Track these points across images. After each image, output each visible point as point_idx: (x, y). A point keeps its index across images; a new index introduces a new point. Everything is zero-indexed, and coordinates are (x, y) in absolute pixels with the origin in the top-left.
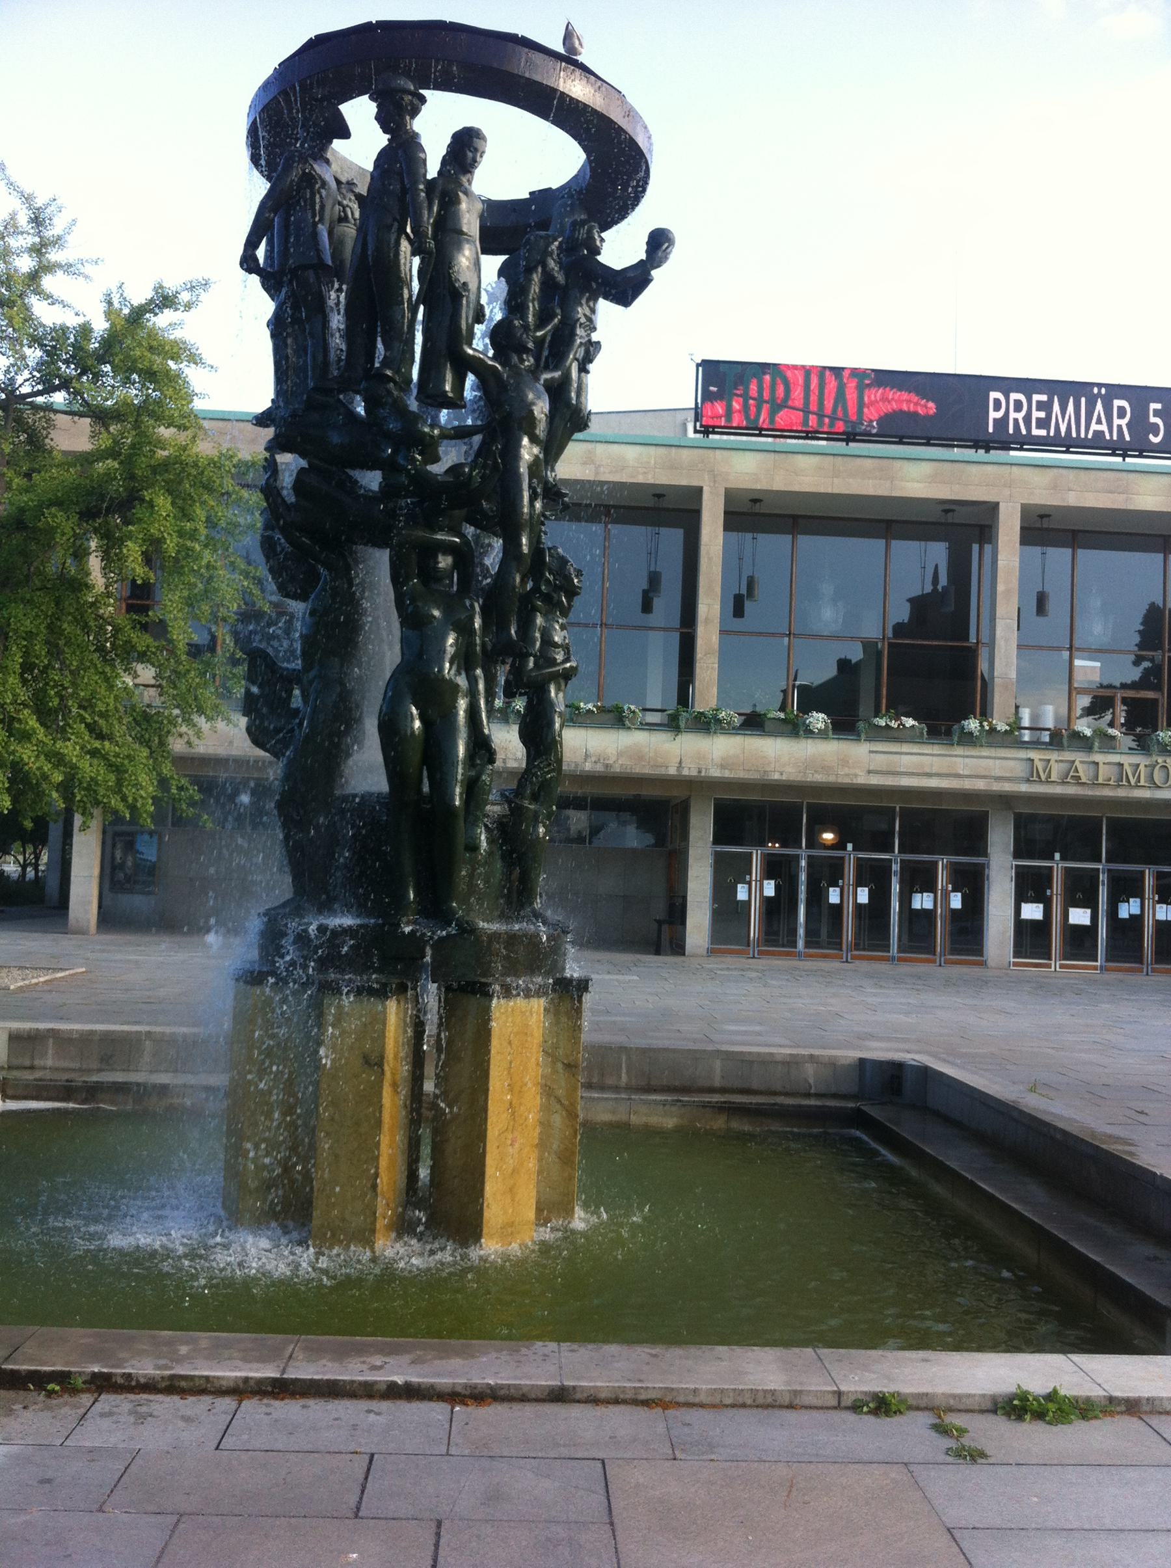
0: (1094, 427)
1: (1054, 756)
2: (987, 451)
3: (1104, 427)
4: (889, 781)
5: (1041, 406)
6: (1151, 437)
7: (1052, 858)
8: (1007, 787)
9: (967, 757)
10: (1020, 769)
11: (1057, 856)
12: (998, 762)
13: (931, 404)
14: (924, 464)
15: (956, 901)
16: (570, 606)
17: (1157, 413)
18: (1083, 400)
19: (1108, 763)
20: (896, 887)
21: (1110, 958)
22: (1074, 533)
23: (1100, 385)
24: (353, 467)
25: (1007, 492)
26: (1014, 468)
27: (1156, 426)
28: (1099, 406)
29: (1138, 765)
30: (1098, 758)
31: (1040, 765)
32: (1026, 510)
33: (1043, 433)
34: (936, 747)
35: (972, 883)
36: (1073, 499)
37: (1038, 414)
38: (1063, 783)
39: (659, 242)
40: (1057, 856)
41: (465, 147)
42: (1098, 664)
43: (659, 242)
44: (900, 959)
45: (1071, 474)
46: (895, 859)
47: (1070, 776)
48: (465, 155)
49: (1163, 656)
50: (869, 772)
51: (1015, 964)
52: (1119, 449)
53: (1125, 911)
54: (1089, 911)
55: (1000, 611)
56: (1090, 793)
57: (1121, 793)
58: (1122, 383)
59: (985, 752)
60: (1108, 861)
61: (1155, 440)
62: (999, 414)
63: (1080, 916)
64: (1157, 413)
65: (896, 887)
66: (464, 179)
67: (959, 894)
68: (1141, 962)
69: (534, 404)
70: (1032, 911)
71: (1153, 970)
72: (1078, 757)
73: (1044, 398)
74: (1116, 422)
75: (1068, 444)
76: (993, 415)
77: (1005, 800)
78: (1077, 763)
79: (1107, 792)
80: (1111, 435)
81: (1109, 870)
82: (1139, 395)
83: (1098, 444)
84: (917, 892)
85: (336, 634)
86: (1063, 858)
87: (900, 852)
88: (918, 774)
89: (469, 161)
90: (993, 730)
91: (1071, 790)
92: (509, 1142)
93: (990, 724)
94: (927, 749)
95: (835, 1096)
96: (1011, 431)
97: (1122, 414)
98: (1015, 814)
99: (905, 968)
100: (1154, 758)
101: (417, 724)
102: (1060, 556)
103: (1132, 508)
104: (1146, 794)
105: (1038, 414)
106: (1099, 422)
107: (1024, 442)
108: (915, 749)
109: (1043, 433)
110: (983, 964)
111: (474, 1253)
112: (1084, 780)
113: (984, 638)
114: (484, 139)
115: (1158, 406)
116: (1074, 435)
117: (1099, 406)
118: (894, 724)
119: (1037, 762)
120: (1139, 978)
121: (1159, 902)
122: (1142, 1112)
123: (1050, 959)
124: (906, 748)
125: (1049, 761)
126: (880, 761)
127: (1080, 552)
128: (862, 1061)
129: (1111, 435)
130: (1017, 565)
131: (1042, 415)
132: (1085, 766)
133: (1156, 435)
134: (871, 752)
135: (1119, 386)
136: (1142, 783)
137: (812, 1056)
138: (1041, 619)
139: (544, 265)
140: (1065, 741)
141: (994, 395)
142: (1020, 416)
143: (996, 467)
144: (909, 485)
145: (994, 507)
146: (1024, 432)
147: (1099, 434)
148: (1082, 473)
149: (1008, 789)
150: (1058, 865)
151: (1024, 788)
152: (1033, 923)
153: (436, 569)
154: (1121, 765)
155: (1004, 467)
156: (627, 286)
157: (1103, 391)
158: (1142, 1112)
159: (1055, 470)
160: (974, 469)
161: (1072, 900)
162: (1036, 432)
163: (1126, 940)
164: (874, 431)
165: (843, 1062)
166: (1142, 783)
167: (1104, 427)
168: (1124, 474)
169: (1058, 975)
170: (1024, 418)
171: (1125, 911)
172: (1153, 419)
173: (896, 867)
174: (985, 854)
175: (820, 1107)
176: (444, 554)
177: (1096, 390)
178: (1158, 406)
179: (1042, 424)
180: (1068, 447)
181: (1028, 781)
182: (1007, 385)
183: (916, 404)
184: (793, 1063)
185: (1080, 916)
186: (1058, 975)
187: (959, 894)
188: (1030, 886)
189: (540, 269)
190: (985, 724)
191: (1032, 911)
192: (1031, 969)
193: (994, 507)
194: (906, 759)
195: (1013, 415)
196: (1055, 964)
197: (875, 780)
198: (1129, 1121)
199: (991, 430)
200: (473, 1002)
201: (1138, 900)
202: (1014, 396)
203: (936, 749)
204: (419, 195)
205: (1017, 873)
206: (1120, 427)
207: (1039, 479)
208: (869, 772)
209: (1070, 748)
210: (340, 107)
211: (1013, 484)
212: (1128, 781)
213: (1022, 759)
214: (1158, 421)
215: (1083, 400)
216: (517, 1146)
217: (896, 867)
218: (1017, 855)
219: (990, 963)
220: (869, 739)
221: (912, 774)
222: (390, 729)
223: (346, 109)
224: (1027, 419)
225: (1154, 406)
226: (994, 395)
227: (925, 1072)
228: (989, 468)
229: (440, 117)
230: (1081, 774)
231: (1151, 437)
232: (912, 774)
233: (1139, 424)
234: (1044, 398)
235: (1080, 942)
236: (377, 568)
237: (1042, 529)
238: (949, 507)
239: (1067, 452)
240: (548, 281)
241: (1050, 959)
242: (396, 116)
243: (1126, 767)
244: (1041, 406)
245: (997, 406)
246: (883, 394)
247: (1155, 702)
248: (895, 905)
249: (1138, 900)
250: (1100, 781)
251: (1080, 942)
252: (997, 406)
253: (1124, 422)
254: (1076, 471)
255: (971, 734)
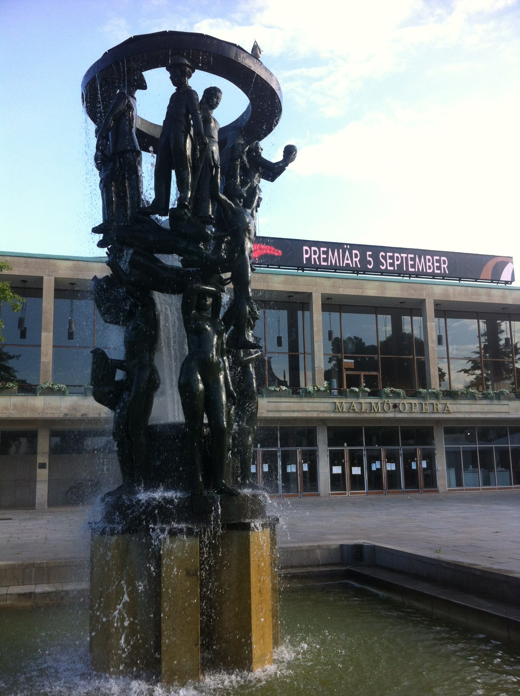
0: (346, 262)
1: (344, 401)
2: (303, 270)
3: (349, 262)
4: (277, 415)
5: (324, 253)
6: (368, 266)
7: (344, 446)
8: (326, 415)
9: (309, 402)
10: (330, 407)
11: (345, 444)
12: (321, 404)
13: (280, 251)
14: (280, 276)
15: (305, 468)
16: (254, 325)
17: (370, 256)
18: (341, 250)
19: (366, 403)
20: (280, 463)
21: (370, 488)
22: (340, 306)
23: (347, 244)
24: (159, 252)
25: (315, 288)
26: (318, 278)
27: (370, 261)
28: (347, 253)
29: (378, 403)
30: (362, 401)
31: (338, 405)
32: (323, 295)
33: (326, 264)
34: (295, 398)
35: (311, 458)
36: (341, 291)
37: (323, 256)
38: (349, 412)
39: (290, 152)
40: (345, 444)
41: (212, 95)
42: (353, 361)
43: (290, 152)
44: (406, 492)
45: (340, 281)
46: (279, 450)
47: (351, 409)
48: (213, 100)
49: (378, 357)
50: (268, 411)
51: (332, 494)
52: (356, 271)
53: (375, 466)
54: (360, 468)
55: (316, 339)
56: (362, 416)
57: (372, 415)
58: (356, 243)
59: (316, 400)
60: (366, 446)
61: (370, 267)
62: (308, 256)
63: (356, 471)
64: (370, 256)
65: (280, 463)
66: (210, 111)
67: (307, 464)
68: (382, 489)
69: (249, 223)
70: (337, 470)
71: (388, 492)
72: (354, 401)
73: (325, 249)
74: (354, 259)
75: (335, 269)
76: (305, 256)
77: (323, 421)
78: (353, 403)
79: (366, 415)
80: (353, 265)
81: (367, 450)
82: (363, 248)
83: (347, 268)
84: (289, 464)
85: (144, 339)
86: (348, 445)
87: (280, 447)
88: (289, 411)
89: (215, 103)
90: (319, 390)
91: (351, 415)
92: (260, 610)
93: (317, 387)
94: (292, 400)
95: (330, 565)
96: (313, 263)
97: (356, 257)
98: (327, 427)
99: (409, 496)
100: (384, 400)
101: (201, 386)
102: (335, 315)
103: (365, 295)
104: (381, 415)
105: (323, 256)
106: (347, 259)
107: (317, 268)
108: (287, 400)
109: (326, 264)
110: (318, 495)
111: (251, 676)
112: (357, 410)
113: (308, 350)
114: (221, 93)
115: (370, 253)
116: (338, 265)
117: (347, 253)
118: (278, 389)
119: (337, 404)
120: (383, 496)
121: (387, 462)
122: (490, 557)
123: (346, 491)
124: (283, 400)
125: (342, 403)
126: (272, 406)
127: (343, 314)
128: (342, 546)
129: (353, 265)
130: (321, 319)
131: (325, 256)
132: (357, 404)
133: (370, 265)
134: (268, 402)
135: (354, 244)
136: (380, 411)
137: (319, 546)
138: (280, 348)
139: (242, 158)
140: (348, 393)
141: (305, 248)
142: (316, 257)
143: (310, 278)
144: (275, 285)
145: (310, 295)
146: (318, 263)
147: (348, 264)
148: (344, 280)
149: (326, 416)
150: (346, 448)
151: (333, 415)
152: (337, 475)
153: (205, 304)
154: (371, 403)
155: (313, 278)
156: (272, 172)
157: (348, 247)
158: (490, 557)
159: (334, 279)
160: (301, 279)
161: (353, 464)
162: (323, 263)
163: (376, 480)
164: (257, 262)
165: (334, 547)
166: (380, 411)
167: (349, 262)
168: (361, 281)
169: (350, 497)
170: (318, 258)
171: (375, 466)
172: (369, 259)
173: (279, 454)
174: (316, 445)
175: (330, 571)
176: (209, 297)
177: (345, 246)
178: (370, 253)
179: (325, 260)
180: (336, 270)
181: (334, 412)
182: (311, 243)
183: (274, 251)
184: (310, 550)
185: (356, 471)
186: (348, 498)
187: (307, 464)
188: (335, 459)
189: (239, 160)
190: (315, 387)
191: (337, 470)
192: (338, 496)
193: (310, 295)
194: (283, 405)
195: (313, 256)
196: (348, 493)
197: (271, 415)
198: (512, 560)
199: (305, 262)
200: (236, 534)
201: (379, 462)
202: (313, 248)
203: (296, 400)
204: (199, 116)
205: (330, 453)
206: (356, 261)
207: (328, 283)
208: (268, 411)
209: (351, 397)
210: (144, 73)
211: (318, 285)
212: (374, 410)
213: (331, 403)
214: (371, 259)
215: (341, 250)
216: (264, 611)
217: (279, 454)
218: (329, 445)
219: (322, 495)
220: (267, 397)
221: (286, 411)
222: (186, 388)
223: (149, 75)
224: (319, 258)
225: (369, 253)
226: (305, 248)
227: (374, 548)
228: (307, 278)
229: (200, 81)
230: (355, 408)
231: (368, 266)
232: (286, 411)
233: (363, 260)
234: (325, 249)
235: (357, 482)
236: (168, 307)
237: (333, 304)
238: (291, 294)
239: (335, 272)
240: (243, 167)
241: (346, 491)
242: (179, 78)
243: (373, 404)
244: (324, 253)
245: (307, 252)
246: (260, 246)
247: (376, 376)
248: (280, 471)
249: (295, 465)
250: (363, 411)
251: (357, 482)
252: (307, 252)
253: (357, 260)
254: (342, 280)
255: (310, 392)
